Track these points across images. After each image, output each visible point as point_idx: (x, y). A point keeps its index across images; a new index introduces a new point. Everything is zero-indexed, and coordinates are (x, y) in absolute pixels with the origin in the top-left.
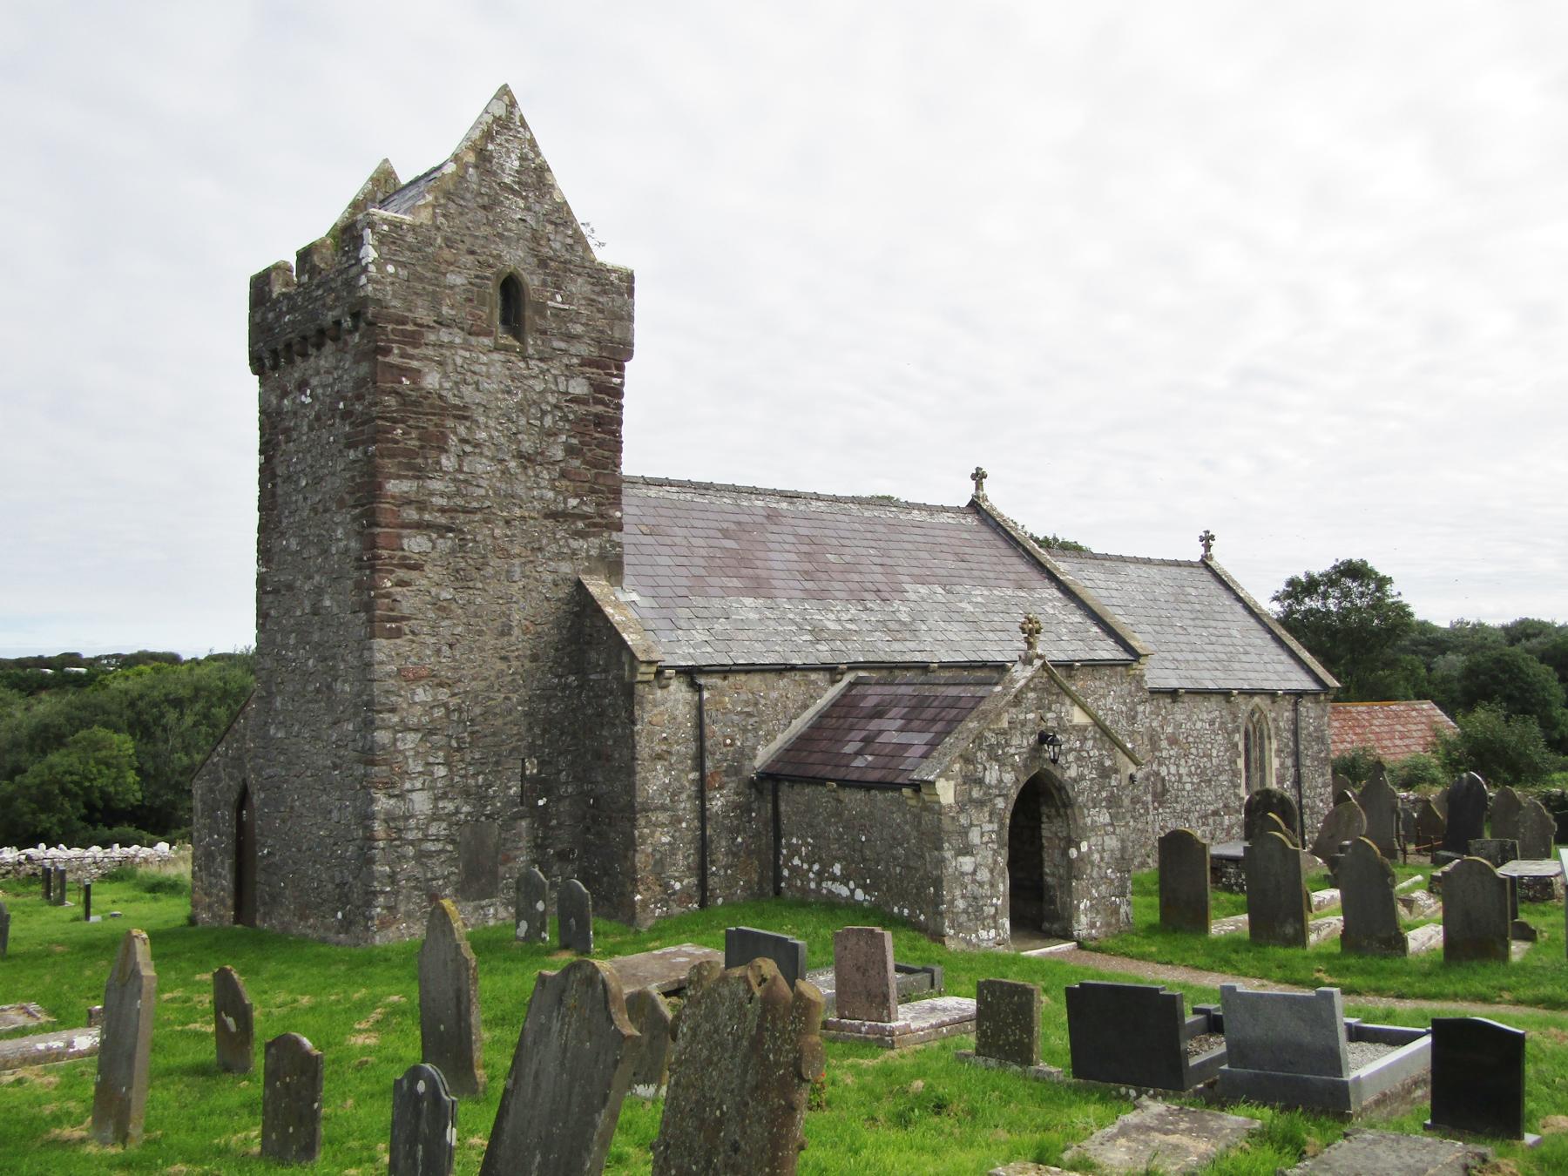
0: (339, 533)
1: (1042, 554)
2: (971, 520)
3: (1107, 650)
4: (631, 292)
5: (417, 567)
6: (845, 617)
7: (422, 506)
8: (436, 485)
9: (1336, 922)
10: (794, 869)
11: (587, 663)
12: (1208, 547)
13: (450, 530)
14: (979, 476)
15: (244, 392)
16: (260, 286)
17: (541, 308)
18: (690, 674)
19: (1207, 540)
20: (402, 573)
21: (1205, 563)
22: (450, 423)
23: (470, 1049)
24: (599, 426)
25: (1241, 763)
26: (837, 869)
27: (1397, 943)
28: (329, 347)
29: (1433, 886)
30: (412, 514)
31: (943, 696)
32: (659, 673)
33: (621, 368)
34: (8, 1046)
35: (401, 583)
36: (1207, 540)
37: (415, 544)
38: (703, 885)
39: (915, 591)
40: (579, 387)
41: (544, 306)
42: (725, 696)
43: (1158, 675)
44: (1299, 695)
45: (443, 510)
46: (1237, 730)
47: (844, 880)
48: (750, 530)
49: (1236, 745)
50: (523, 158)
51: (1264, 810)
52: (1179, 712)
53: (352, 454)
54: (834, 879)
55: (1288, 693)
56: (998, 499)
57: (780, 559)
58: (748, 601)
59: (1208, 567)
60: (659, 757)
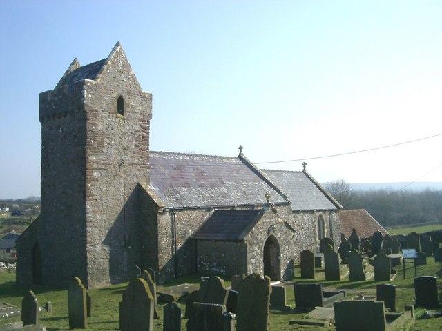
0: (73, 170)
1: (265, 175)
2: (239, 161)
3: (281, 200)
4: (151, 99)
5: (97, 181)
6: (210, 192)
7: (97, 163)
8: (102, 157)
9: (348, 273)
10: (201, 265)
11: (140, 210)
12: (305, 167)
13: (105, 170)
14: (241, 148)
15: (37, 127)
16: (44, 97)
17: (128, 105)
18: (172, 211)
19: (304, 165)
20: (93, 183)
21: (304, 172)
22: (105, 139)
23: (186, 309)
24: (145, 139)
25: (316, 231)
26: (215, 264)
27: (363, 277)
28: (68, 116)
29: (371, 262)
30: (95, 165)
31: (250, 216)
32: (164, 210)
33: (149, 122)
34: (106, 312)
35: (92, 186)
36: (304, 165)
37: (97, 174)
38: (176, 269)
39: (228, 184)
40: (138, 128)
41: (129, 104)
42: (181, 216)
43: (295, 207)
44: (331, 211)
45: (103, 164)
46: (315, 221)
47: (217, 267)
48: (184, 168)
49: (315, 226)
50: (124, 63)
51: (325, 244)
52: (300, 216)
53: (78, 148)
54: (214, 266)
55: (329, 210)
56: (246, 154)
57: (191, 175)
58: (184, 188)
59: (305, 173)
60: (164, 234)
